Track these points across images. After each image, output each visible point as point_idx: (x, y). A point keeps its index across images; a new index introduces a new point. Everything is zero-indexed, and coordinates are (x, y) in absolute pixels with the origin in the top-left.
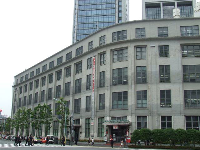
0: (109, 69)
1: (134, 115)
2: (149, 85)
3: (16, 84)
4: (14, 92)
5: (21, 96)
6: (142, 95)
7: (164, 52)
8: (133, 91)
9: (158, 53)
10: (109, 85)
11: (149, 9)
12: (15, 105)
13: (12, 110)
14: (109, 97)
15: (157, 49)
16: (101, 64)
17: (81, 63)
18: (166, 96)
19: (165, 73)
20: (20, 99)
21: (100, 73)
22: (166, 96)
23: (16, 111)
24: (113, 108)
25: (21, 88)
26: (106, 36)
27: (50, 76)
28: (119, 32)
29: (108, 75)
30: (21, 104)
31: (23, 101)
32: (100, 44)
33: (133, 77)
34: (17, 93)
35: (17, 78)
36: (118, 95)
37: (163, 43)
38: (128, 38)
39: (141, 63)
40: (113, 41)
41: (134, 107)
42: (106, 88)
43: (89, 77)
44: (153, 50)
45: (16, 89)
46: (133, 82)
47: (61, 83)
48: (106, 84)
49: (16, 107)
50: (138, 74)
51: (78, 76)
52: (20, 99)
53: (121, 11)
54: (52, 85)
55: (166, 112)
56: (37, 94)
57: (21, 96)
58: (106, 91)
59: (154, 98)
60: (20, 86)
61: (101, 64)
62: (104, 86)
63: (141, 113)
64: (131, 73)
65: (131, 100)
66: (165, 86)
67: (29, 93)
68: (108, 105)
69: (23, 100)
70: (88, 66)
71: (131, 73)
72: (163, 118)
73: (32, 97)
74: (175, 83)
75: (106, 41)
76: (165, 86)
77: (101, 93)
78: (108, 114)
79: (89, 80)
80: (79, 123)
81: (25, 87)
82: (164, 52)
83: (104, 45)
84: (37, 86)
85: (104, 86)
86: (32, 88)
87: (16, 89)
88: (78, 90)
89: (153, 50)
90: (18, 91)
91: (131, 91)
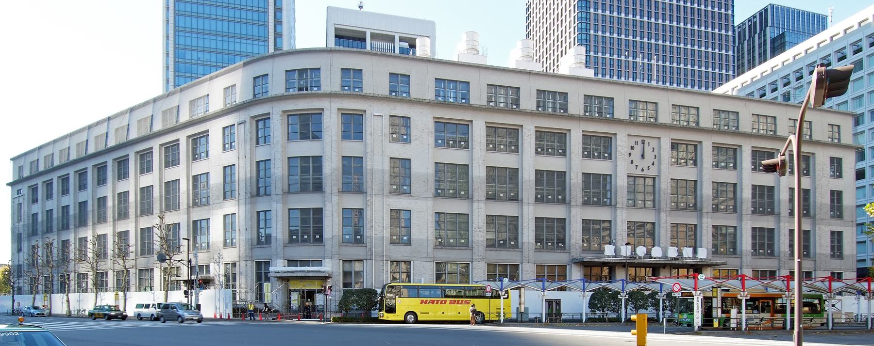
0: (278, 156)
3: (17, 178)
4: (13, 199)
5: (36, 208)
8: (335, 208)
9: (387, 130)
10: (280, 192)
11: (341, 40)
12: (22, 231)
13: (12, 243)
14: (280, 218)
15: (387, 121)
16: (258, 143)
17: (205, 134)
18: (400, 220)
19: (401, 174)
20: (35, 216)
21: (258, 163)
22: (400, 220)
23: (25, 245)
25: (34, 189)
26: (270, 76)
27: (80, 174)
28: (302, 71)
29: (279, 169)
30: (55, 223)
31: (42, 222)
32: (255, 95)
33: (334, 177)
34: (25, 201)
35: (21, 162)
37: (401, 110)
38: (325, 89)
40: (287, 89)
41: (336, 242)
42: (273, 197)
43: (228, 170)
45: (19, 191)
46: (335, 190)
47: (68, 200)
48: (273, 189)
49: (24, 236)
51: (199, 168)
52: (35, 216)
53: (281, 35)
54: (68, 200)
55: (400, 252)
56: (65, 209)
57: (36, 208)
58: (274, 204)
60: (32, 182)
61: (258, 143)
62: (37, 234)
66: (401, 203)
67: (59, 201)
68: (280, 237)
69: (45, 218)
70: (224, 145)
73: (40, 219)
74: (419, 198)
75: (269, 85)
76: (401, 203)
77: (34, 243)
78: (281, 254)
79: (228, 179)
80: (208, 271)
81: (60, 181)
83: (265, 97)
84: (65, 191)
85: (37, 234)
86: (52, 194)
87: (19, 191)
88: (199, 200)
90: (26, 196)
91: (333, 207)
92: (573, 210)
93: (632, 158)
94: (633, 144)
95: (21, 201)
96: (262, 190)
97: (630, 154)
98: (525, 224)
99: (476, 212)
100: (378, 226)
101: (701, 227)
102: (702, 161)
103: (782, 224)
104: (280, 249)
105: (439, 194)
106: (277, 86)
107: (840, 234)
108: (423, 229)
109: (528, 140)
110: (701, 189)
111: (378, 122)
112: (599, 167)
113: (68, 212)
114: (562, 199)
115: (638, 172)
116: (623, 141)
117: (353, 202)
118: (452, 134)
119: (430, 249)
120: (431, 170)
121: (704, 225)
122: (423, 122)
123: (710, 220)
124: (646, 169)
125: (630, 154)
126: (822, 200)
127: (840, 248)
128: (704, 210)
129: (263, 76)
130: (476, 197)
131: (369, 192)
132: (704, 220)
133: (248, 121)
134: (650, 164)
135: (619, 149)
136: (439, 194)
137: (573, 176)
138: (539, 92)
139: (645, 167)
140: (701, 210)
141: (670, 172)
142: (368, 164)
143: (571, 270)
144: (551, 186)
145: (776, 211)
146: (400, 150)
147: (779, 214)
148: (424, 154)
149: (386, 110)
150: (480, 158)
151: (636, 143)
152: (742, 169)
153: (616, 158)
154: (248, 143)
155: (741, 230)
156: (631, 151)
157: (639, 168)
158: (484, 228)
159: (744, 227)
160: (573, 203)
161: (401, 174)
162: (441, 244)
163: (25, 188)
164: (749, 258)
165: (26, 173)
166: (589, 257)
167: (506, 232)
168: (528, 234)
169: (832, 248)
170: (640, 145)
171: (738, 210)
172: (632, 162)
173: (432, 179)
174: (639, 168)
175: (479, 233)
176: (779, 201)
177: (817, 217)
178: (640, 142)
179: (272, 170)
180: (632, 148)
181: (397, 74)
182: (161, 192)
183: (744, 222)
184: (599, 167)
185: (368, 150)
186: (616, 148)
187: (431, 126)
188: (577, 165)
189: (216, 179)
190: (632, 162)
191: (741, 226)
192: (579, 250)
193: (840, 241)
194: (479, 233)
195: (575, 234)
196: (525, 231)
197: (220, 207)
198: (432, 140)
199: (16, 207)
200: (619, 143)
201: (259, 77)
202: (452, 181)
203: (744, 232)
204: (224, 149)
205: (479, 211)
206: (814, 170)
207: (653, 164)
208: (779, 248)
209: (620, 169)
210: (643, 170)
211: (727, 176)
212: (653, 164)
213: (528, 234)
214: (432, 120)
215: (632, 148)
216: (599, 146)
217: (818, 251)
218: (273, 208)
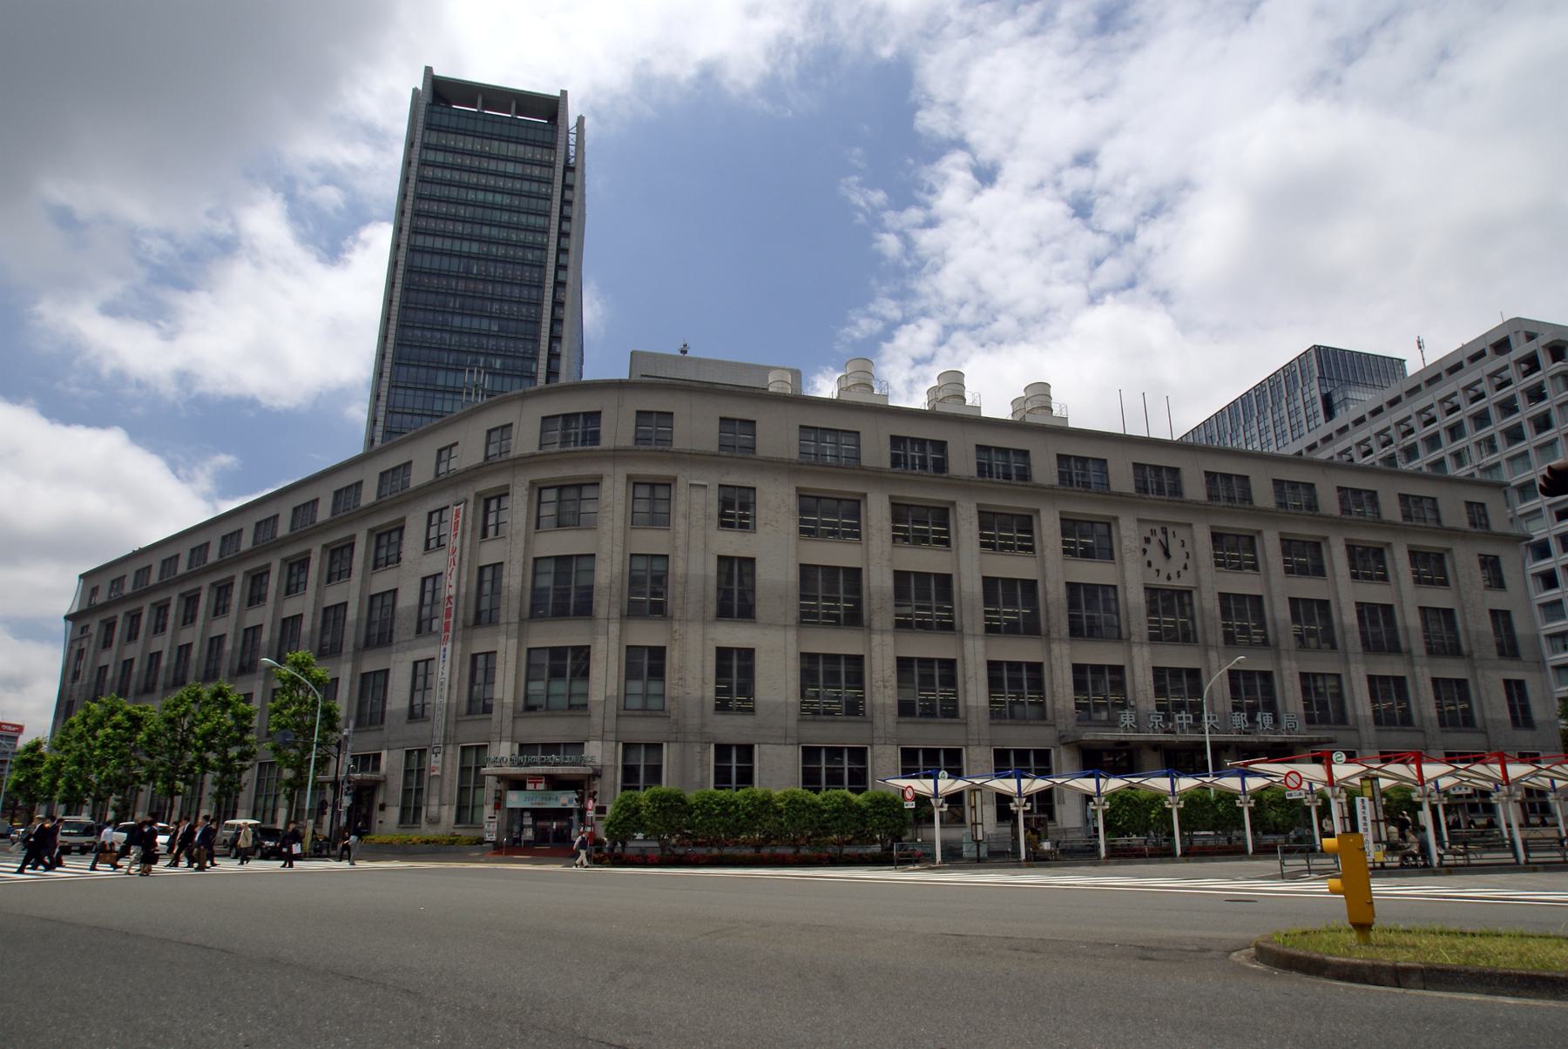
0: (518, 555)
1: (612, 736)
2: (676, 626)
3: (85, 607)
6: (648, 664)
7: (736, 510)
8: (614, 646)
10: (515, 618)
15: (713, 496)
16: (484, 535)
18: (735, 670)
19: (735, 591)
22: (735, 670)
24: (997, 713)
30: (161, 678)
31: (114, 679)
34: (90, 646)
36: (552, 658)
39: (650, 541)
41: (612, 708)
42: (503, 628)
44: (695, 501)
45: (84, 629)
46: (615, 613)
48: (503, 613)
50: (635, 581)
55: (732, 728)
59: (692, 674)
63: (642, 730)
64: (608, 574)
65: (605, 679)
66: (735, 635)
71: (608, 574)
72: (722, 751)
74: (769, 625)
75: (513, 441)
76: (735, 635)
78: (507, 732)
82: (736, 510)
87: (84, 629)
88: (379, 636)
89: (695, 501)
90: (94, 638)
92: (1056, 648)
93: (1148, 557)
94: (1148, 535)
95: (85, 644)
96: (485, 616)
97: (1145, 551)
98: (970, 673)
99: (877, 651)
100: (692, 674)
101: (1281, 676)
102: (1266, 563)
103: (1417, 669)
104: (507, 722)
105: (807, 618)
106: (525, 440)
107: (1520, 684)
108: (777, 681)
109: (966, 526)
110: (1272, 610)
111: (698, 497)
112: (1090, 572)
113: (158, 662)
114: (1031, 627)
115: (1162, 582)
116: (1128, 533)
117: (647, 634)
118: (827, 515)
119: (792, 721)
120: (793, 575)
121: (1286, 673)
122: (776, 503)
123: (1294, 664)
124: (1173, 576)
125: (1145, 551)
126: (1476, 626)
127: (1526, 709)
128: (1283, 646)
129: (504, 427)
130: (876, 625)
131: (677, 615)
132: (1285, 663)
133: (471, 499)
134: (1181, 568)
135: (1126, 542)
136: (807, 618)
137: (1050, 588)
138: (980, 448)
139: (1171, 575)
140: (1277, 645)
141: (1211, 584)
142: (677, 567)
143: (1058, 757)
144: (1012, 604)
145: (1403, 645)
146: (734, 543)
147: (1409, 652)
148: (777, 550)
149: (712, 479)
150: (878, 557)
151: (1153, 532)
152: (1334, 576)
153: (1121, 558)
154: (468, 535)
155: (1350, 680)
156: (1146, 546)
157: (1163, 575)
158: (894, 681)
159: (1353, 674)
160: (1054, 635)
161: (735, 591)
162: (810, 710)
163: (95, 626)
164: (1372, 729)
165: (101, 598)
166: (1089, 735)
167: (930, 685)
168: (975, 692)
169: (1512, 709)
170: (1160, 535)
171: (1339, 646)
172: (1149, 564)
173: (794, 592)
174: (1163, 575)
175: (882, 688)
176: (1406, 629)
177: (1476, 655)
178: (1159, 531)
179: (505, 581)
180: (1147, 540)
181: (734, 420)
182: (313, 625)
183: (1353, 667)
184: (1090, 572)
185: (680, 542)
186: (1120, 542)
187: (792, 502)
188: (1052, 569)
189: (408, 599)
190: (1149, 564)
191: (1349, 673)
192: (1072, 721)
193: (1523, 694)
194: (882, 688)
195: (1061, 690)
196: (971, 686)
197: (409, 649)
198: (793, 526)
199: (74, 654)
200: (1123, 532)
201: (496, 429)
202: (831, 596)
203: (1355, 683)
204: (427, 548)
205: (882, 652)
206: (1456, 576)
207: (1185, 567)
208: (1420, 711)
209: (1130, 575)
210: (1169, 578)
211: (1308, 588)
212: (1185, 567)
213: (975, 692)
214: (793, 492)
215: (1147, 540)
216: (1087, 540)
217: (1488, 715)
218: (500, 649)
